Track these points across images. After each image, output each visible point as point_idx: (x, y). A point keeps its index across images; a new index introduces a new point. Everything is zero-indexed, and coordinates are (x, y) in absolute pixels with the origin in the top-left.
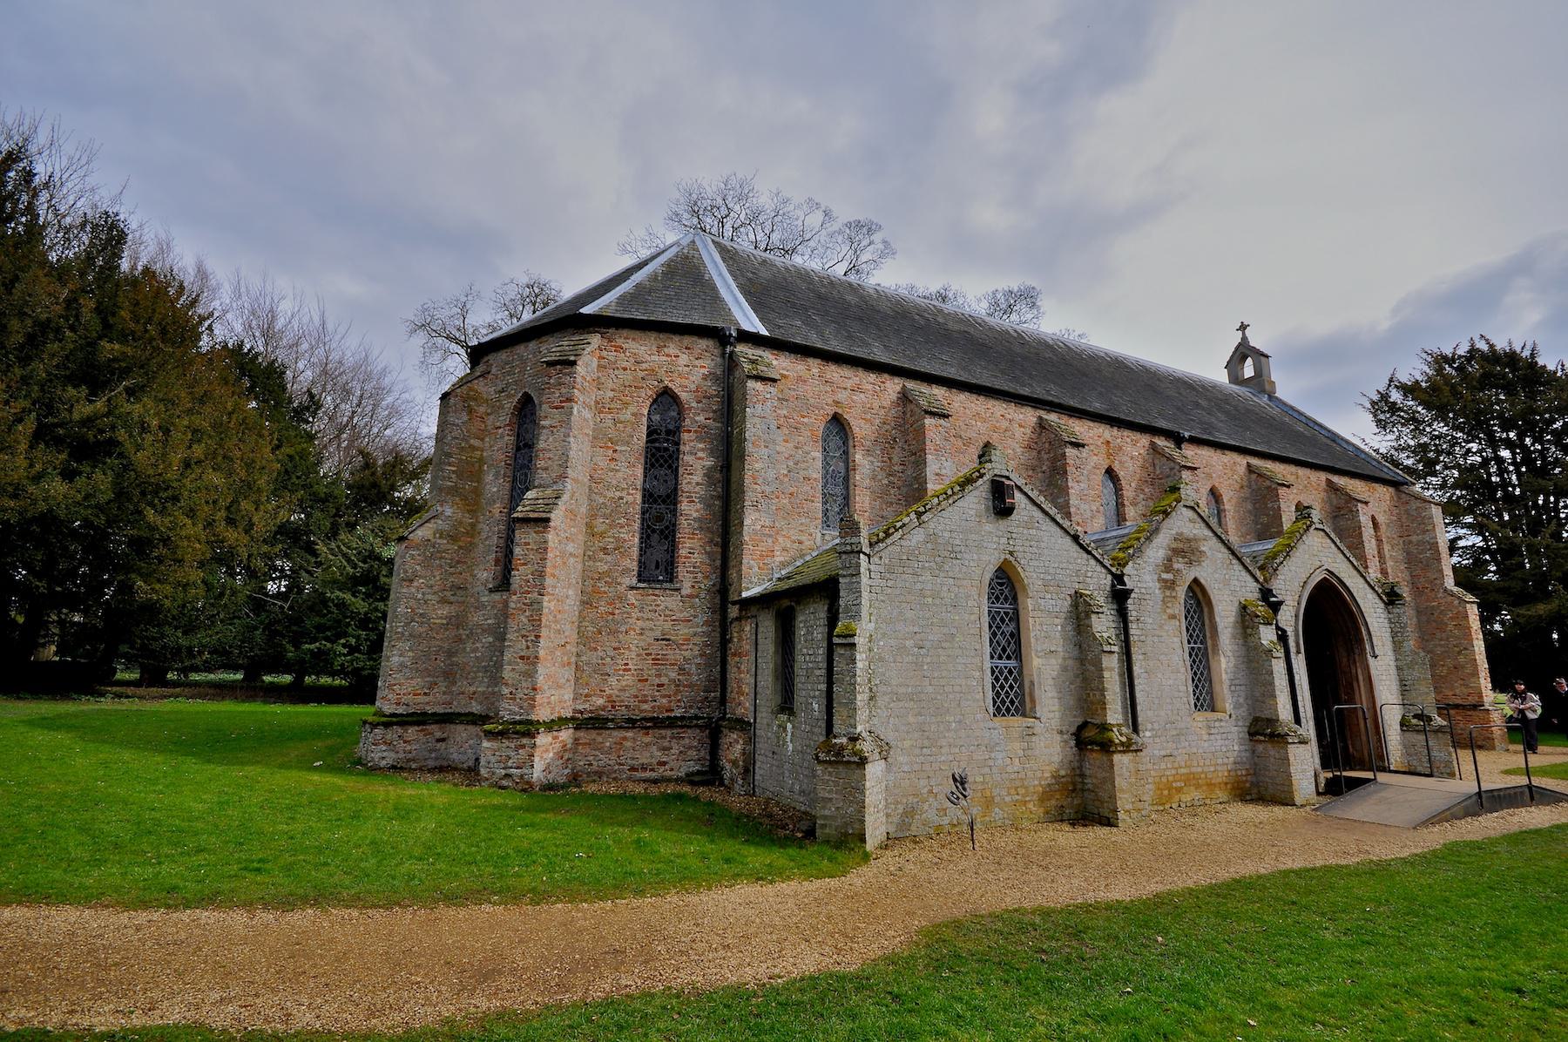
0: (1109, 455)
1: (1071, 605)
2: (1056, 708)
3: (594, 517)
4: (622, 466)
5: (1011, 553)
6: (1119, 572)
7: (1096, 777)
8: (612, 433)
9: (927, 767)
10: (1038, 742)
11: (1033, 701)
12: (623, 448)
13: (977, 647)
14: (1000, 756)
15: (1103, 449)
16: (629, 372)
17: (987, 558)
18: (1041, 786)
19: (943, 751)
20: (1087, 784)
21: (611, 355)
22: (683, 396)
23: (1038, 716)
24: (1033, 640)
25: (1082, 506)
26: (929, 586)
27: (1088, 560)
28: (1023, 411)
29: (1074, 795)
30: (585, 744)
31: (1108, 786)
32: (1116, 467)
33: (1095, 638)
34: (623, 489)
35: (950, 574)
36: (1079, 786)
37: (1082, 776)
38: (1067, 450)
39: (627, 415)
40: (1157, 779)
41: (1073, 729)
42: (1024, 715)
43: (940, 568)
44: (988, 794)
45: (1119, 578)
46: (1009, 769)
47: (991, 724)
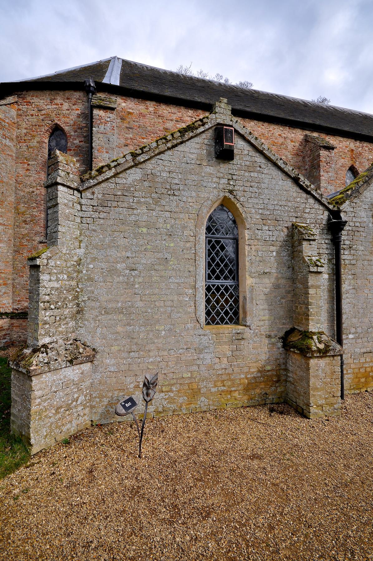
0: (352, 158)
1: (287, 236)
2: (267, 317)
3: (18, 203)
4: (33, 173)
5: (231, 192)
6: (336, 209)
7: (296, 374)
8: (26, 154)
9: (135, 367)
10: (246, 344)
11: (245, 313)
12: (33, 163)
13: (191, 269)
14: (208, 356)
15: (349, 155)
16: (34, 117)
17: (206, 195)
18: (247, 378)
19: (151, 354)
20: (289, 377)
21: (24, 108)
22: (66, 128)
23: (248, 324)
24: (247, 264)
25: (329, 187)
26: (145, 218)
27: (307, 199)
28: (294, 131)
29: (277, 385)
30: (17, 326)
31: (304, 384)
32: (357, 166)
33: (304, 261)
34: (34, 187)
35: (167, 208)
36: (283, 378)
37: (286, 370)
38: (321, 152)
39: (34, 143)
40: (357, 371)
41: (281, 334)
42: (237, 323)
43: (156, 203)
44: (195, 386)
45: (335, 214)
46: (217, 367)
47: (201, 332)
